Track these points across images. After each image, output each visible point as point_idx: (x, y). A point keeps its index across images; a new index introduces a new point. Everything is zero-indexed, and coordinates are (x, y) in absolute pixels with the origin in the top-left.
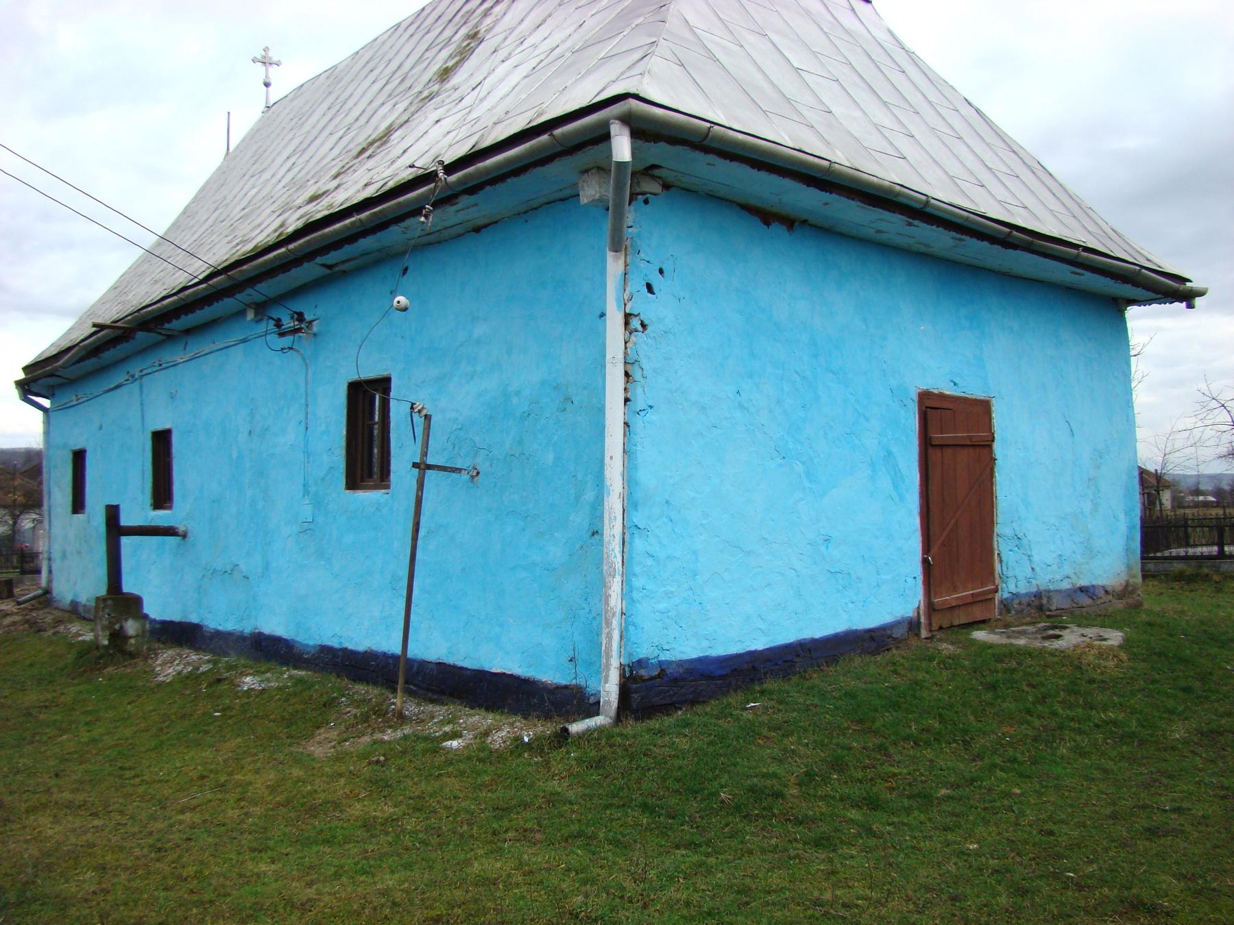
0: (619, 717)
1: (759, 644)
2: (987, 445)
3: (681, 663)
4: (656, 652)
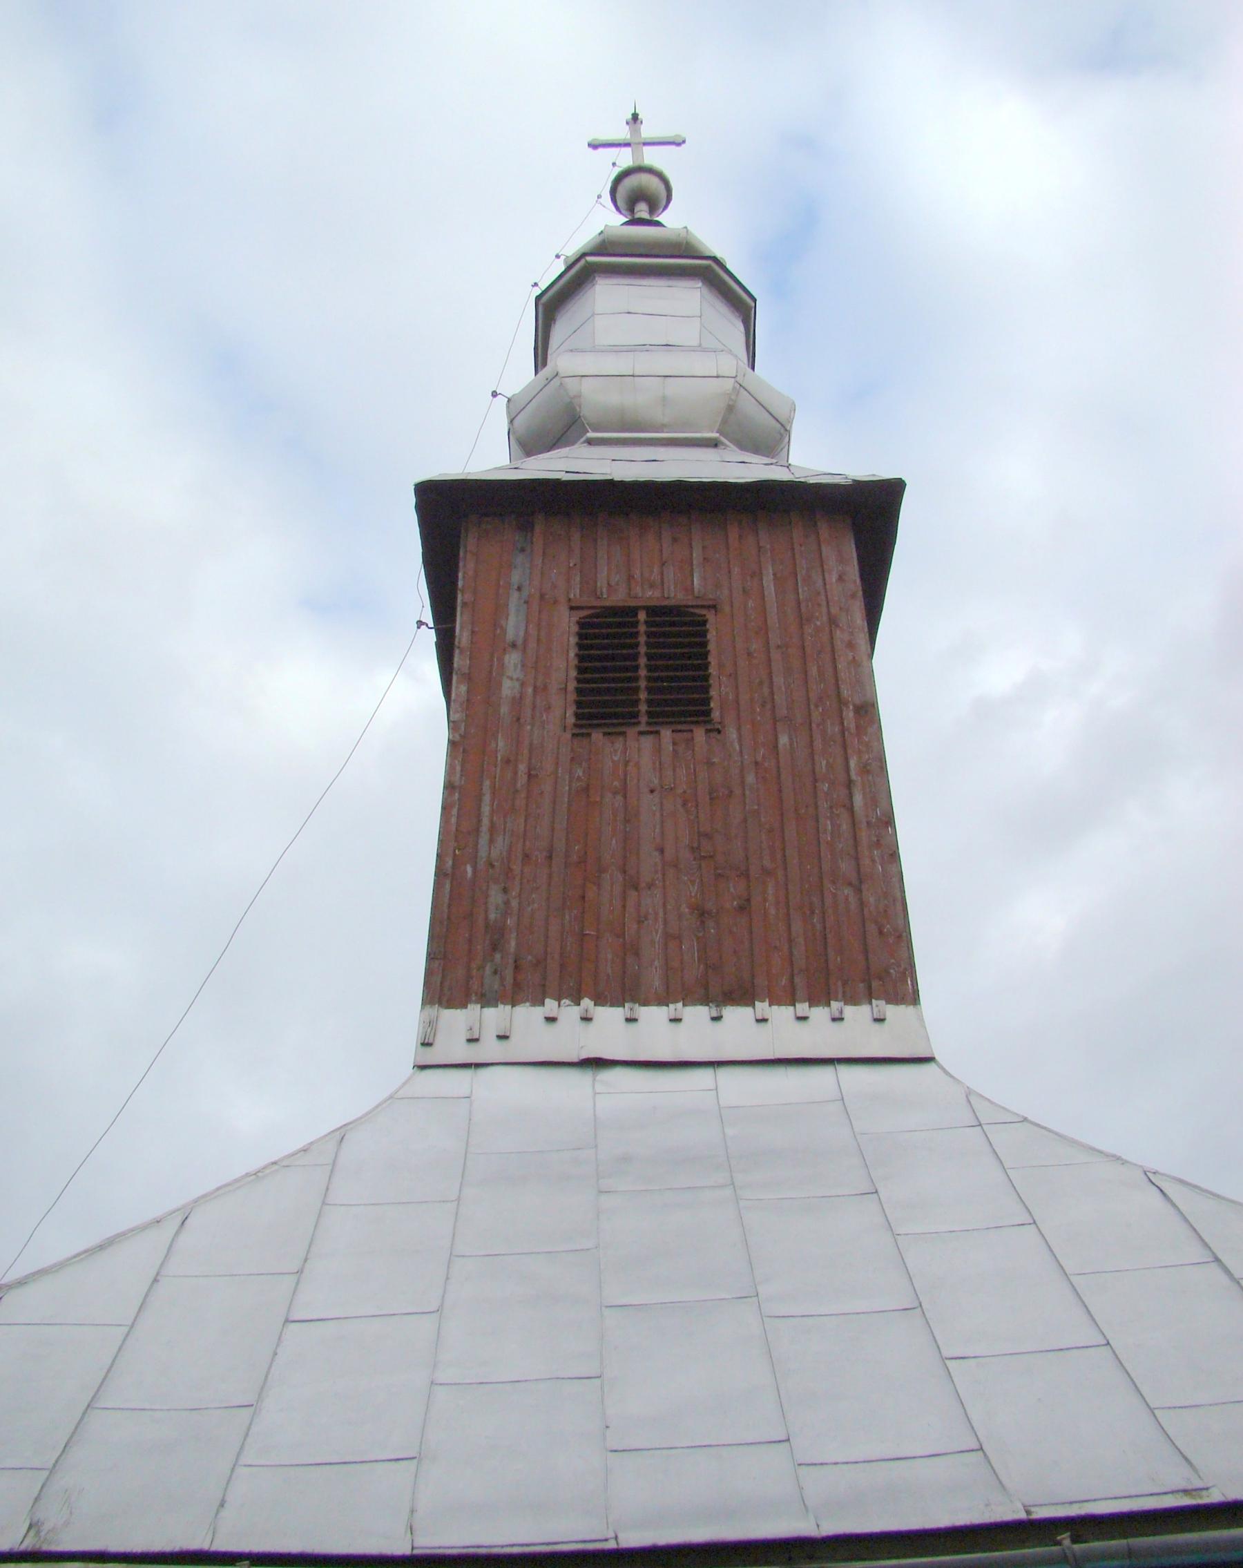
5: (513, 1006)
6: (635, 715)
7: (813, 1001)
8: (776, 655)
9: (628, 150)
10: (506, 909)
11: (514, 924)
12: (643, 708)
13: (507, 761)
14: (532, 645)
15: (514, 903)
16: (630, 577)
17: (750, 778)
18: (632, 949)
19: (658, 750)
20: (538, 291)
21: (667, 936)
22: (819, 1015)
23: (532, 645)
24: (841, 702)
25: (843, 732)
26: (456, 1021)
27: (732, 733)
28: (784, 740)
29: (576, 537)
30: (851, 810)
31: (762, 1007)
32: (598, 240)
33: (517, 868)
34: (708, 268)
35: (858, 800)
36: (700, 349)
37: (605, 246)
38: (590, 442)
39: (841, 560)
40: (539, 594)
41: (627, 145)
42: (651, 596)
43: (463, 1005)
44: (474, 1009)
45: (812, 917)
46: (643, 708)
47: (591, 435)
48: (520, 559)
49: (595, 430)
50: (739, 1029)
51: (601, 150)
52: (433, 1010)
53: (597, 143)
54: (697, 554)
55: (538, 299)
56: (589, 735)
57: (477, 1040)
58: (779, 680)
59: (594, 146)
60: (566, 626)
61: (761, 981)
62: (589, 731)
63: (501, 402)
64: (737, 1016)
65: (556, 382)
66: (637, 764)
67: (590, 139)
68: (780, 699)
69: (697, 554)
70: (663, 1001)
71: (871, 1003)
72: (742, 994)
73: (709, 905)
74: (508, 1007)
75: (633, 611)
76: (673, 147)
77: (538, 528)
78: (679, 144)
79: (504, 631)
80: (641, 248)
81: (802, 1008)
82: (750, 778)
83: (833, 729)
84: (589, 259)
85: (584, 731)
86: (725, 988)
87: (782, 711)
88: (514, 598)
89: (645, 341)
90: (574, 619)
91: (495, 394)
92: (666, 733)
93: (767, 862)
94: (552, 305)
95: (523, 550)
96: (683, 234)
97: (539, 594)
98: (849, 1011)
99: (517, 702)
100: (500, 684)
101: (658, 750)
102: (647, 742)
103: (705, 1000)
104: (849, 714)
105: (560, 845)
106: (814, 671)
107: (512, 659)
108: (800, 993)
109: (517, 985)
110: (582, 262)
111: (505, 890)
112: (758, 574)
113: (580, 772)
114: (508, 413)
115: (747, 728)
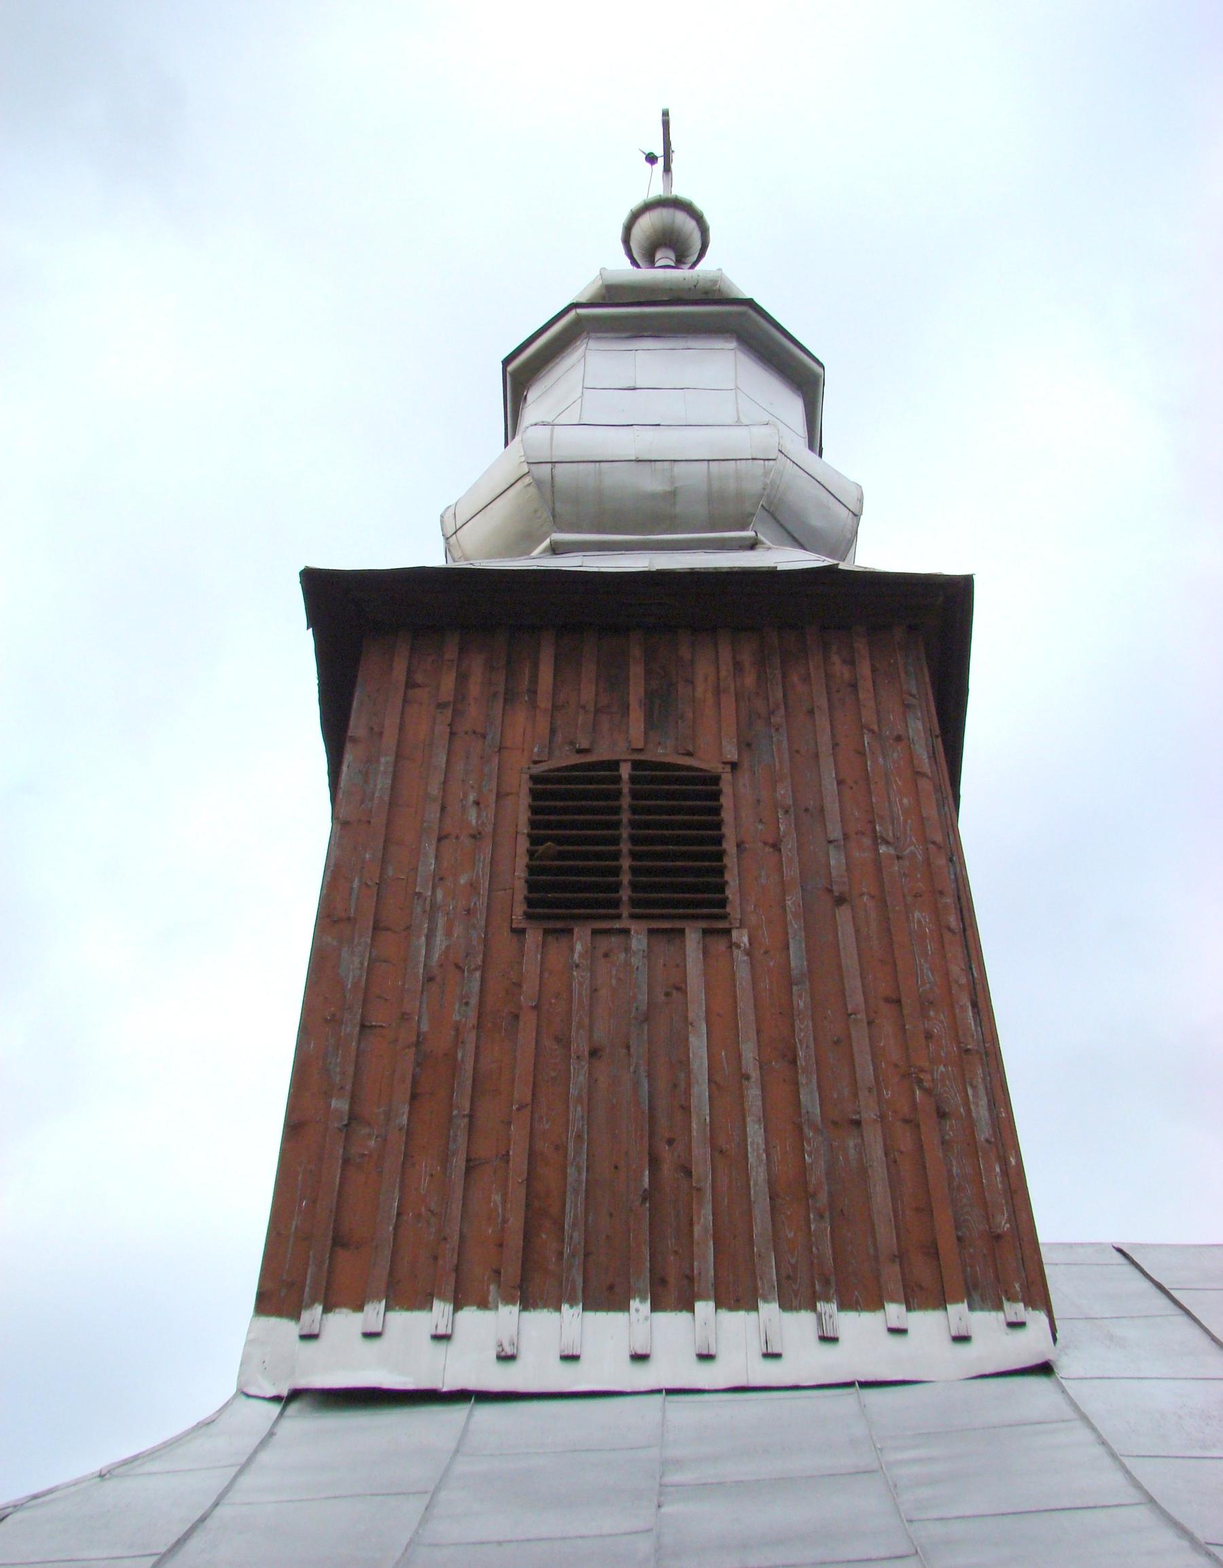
5: (909, 1309)
6: (616, 904)
12: (625, 894)
29: (861, 645)
36: (738, 424)
37: (611, 294)
40: (506, 742)
44: (571, 1314)
46: (625, 894)
56: (570, 931)
57: (777, 1356)
62: (678, 924)
71: (814, 1309)
74: (515, 1309)
75: (614, 765)
80: (664, 293)
84: (581, 311)
85: (560, 925)
89: (668, 413)
94: (523, 373)
96: (715, 282)
97: (506, 742)
98: (400, 1320)
110: (572, 314)
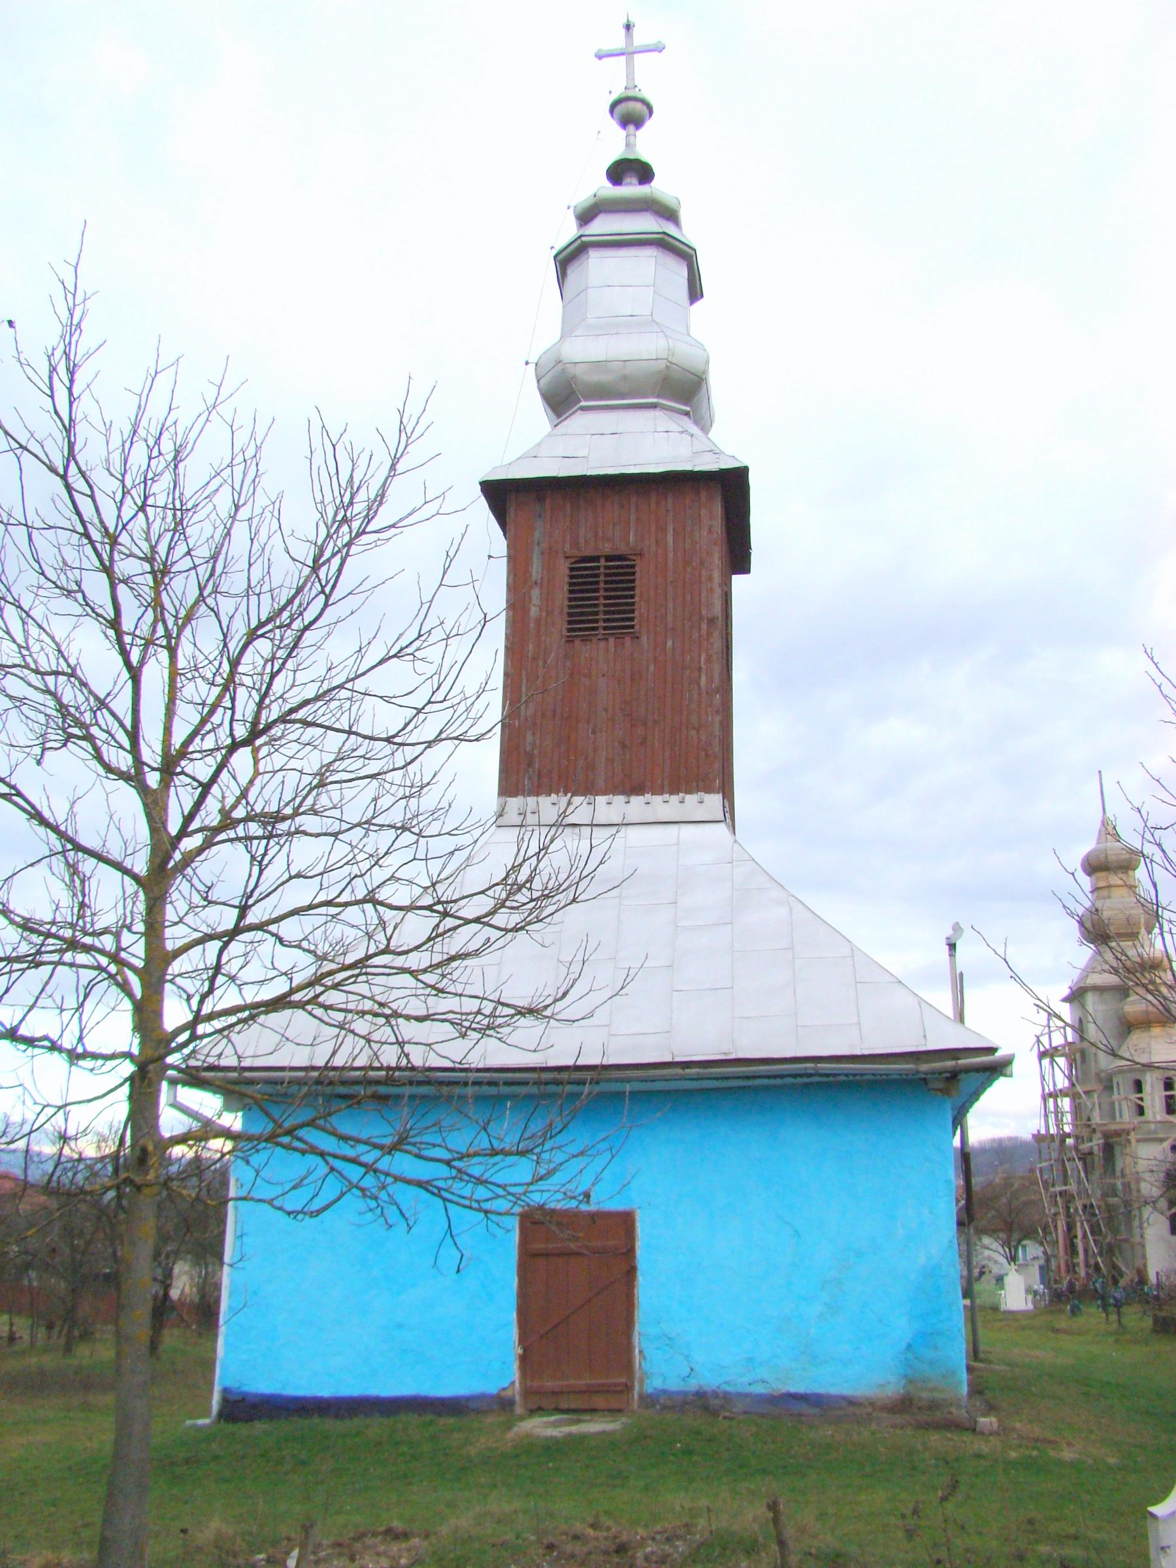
0: (212, 1423)
1: (325, 1392)
2: (630, 1252)
3: (257, 1395)
4: (237, 1385)
7: (671, 793)
8: (670, 589)
9: (623, 58)
10: (533, 745)
11: (547, 754)
13: (533, 659)
14: (545, 585)
15: (538, 742)
16: (596, 536)
17: (652, 668)
18: (591, 767)
19: (607, 650)
20: (554, 252)
21: (607, 759)
22: (674, 799)
23: (545, 585)
24: (701, 619)
25: (700, 637)
26: (514, 803)
27: (644, 639)
28: (670, 643)
30: (699, 686)
31: (648, 796)
32: (592, 201)
33: (538, 722)
34: (662, 240)
35: (703, 679)
38: (583, 409)
39: (712, 517)
41: (622, 54)
42: (607, 548)
43: (516, 796)
45: (683, 749)
47: (583, 404)
48: (539, 523)
49: (586, 399)
50: (637, 807)
51: (605, 60)
52: (503, 799)
53: (602, 53)
54: (633, 518)
55: (555, 257)
58: (670, 606)
59: (600, 57)
60: (563, 568)
61: (648, 784)
63: (532, 367)
64: (637, 801)
65: (560, 366)
66: (597, 661)
67: (595, 50)
68: (670, 618)
69: (633, 518)
70: (605, 793)
72: (637, 789)
73: (627, 742)
76: (656, 53)
77: (548, 501)
78: (660, 51)
79: (531, 576)
81: (666, 796)
82: (652, 668)
83: (695, 636)
86: (633, 787)
87: (670, 625)
88: (536, 548)
90: (568, 565)
91: (527, 363)
92: (612, 640)
93: (656, 717)
95: (540, 516)
98: (688, 798)
99: (538, 621)
100: (529, 611)
101: (607, 650)
102: (602, 644)
103: (623, 793)
104: (704, 626)
105: (559, 711)
106: (688, 597)
107: (535, 593)
108: (666, 789)
109: (539, 786)
110: (579, 242)
111: (533, 734)
112: (664, 530)
113: (568, 664)
114: (537, 375)
115: (652, 636)
